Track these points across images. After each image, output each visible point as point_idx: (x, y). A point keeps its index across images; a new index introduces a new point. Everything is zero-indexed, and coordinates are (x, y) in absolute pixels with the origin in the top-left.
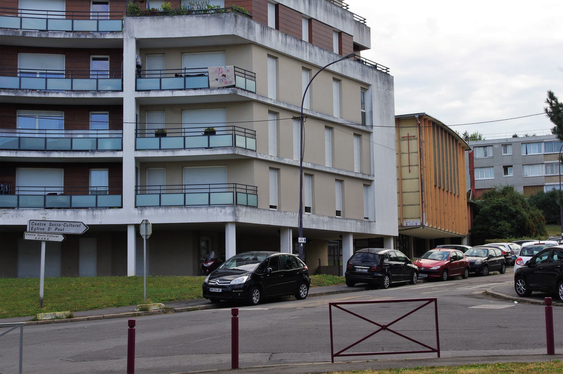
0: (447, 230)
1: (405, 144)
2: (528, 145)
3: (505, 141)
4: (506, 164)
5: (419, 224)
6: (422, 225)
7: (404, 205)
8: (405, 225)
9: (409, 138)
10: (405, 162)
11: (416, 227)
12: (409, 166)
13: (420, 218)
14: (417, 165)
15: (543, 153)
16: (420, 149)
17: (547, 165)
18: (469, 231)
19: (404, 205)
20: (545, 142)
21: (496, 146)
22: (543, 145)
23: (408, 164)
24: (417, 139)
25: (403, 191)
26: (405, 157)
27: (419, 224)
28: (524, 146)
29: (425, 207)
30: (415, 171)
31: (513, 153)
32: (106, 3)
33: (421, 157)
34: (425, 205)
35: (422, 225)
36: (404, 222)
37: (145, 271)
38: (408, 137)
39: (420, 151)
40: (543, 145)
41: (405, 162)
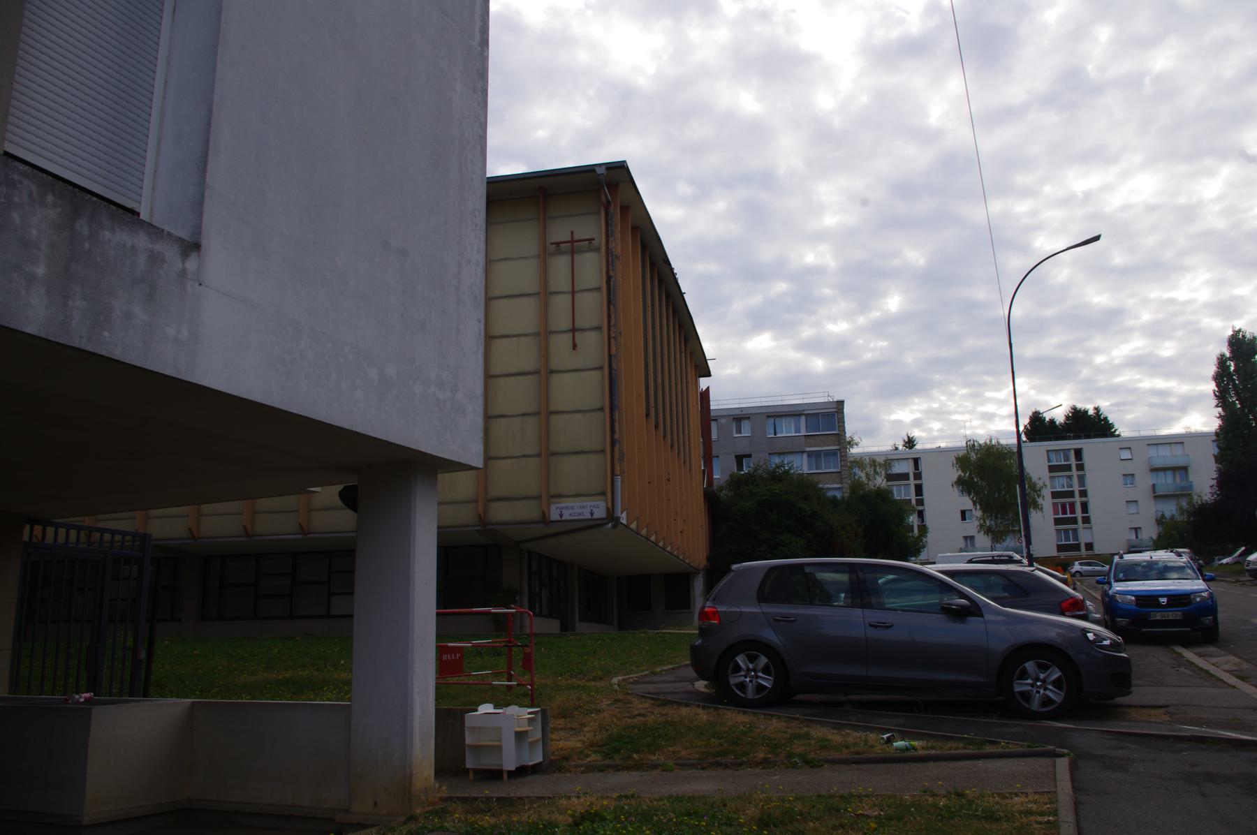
0: (669, 549)
1: (560, 264)
2: (778, 420)
3: (738, 412)
4: (741, 451)
5: (600, 513)
6: (611, 517)
7: (551, 413)
8: (554, 516)
9: (573, 247)
10: (561, 320)
11: (592, 525)
12: (574, 330)
13: (604, 494)
14: (598, 328)
15: (803, 433)
16: (609, 278)
17: (810, 454)
18: (708, 559)
19: (553, 454)
20: (807, 415)
21: (723, 421)
22: (803, 419)
23: (569, 326)
24: (598, 250)
25: (553, 408)
26: (561, 305)
27: (600, 513)
28: (771, 421)
29: (622, 460)
30: (592, 343)
31: (753, 431)
32: (7, 154)
33: (609, 302)
34: (622, 453)
35: (611, 517)
36: (553, 507)
37: (792, 611)
38: (572, 241)
39: (608, 283)
40: (803, 419)
41: (561, 320)
